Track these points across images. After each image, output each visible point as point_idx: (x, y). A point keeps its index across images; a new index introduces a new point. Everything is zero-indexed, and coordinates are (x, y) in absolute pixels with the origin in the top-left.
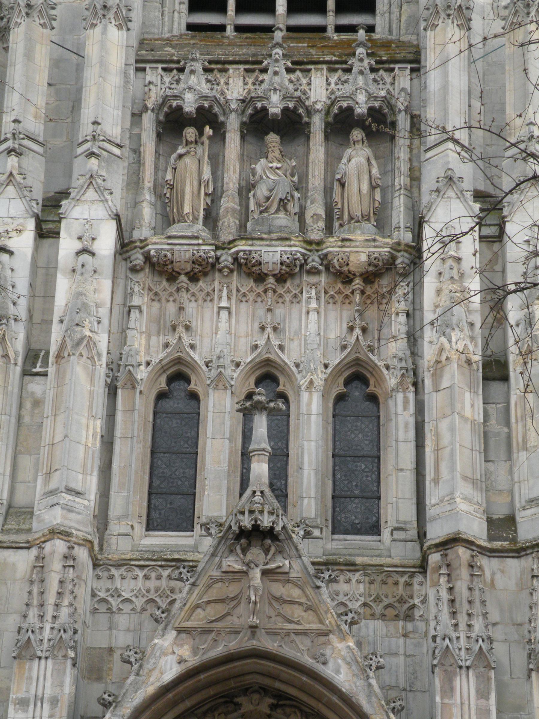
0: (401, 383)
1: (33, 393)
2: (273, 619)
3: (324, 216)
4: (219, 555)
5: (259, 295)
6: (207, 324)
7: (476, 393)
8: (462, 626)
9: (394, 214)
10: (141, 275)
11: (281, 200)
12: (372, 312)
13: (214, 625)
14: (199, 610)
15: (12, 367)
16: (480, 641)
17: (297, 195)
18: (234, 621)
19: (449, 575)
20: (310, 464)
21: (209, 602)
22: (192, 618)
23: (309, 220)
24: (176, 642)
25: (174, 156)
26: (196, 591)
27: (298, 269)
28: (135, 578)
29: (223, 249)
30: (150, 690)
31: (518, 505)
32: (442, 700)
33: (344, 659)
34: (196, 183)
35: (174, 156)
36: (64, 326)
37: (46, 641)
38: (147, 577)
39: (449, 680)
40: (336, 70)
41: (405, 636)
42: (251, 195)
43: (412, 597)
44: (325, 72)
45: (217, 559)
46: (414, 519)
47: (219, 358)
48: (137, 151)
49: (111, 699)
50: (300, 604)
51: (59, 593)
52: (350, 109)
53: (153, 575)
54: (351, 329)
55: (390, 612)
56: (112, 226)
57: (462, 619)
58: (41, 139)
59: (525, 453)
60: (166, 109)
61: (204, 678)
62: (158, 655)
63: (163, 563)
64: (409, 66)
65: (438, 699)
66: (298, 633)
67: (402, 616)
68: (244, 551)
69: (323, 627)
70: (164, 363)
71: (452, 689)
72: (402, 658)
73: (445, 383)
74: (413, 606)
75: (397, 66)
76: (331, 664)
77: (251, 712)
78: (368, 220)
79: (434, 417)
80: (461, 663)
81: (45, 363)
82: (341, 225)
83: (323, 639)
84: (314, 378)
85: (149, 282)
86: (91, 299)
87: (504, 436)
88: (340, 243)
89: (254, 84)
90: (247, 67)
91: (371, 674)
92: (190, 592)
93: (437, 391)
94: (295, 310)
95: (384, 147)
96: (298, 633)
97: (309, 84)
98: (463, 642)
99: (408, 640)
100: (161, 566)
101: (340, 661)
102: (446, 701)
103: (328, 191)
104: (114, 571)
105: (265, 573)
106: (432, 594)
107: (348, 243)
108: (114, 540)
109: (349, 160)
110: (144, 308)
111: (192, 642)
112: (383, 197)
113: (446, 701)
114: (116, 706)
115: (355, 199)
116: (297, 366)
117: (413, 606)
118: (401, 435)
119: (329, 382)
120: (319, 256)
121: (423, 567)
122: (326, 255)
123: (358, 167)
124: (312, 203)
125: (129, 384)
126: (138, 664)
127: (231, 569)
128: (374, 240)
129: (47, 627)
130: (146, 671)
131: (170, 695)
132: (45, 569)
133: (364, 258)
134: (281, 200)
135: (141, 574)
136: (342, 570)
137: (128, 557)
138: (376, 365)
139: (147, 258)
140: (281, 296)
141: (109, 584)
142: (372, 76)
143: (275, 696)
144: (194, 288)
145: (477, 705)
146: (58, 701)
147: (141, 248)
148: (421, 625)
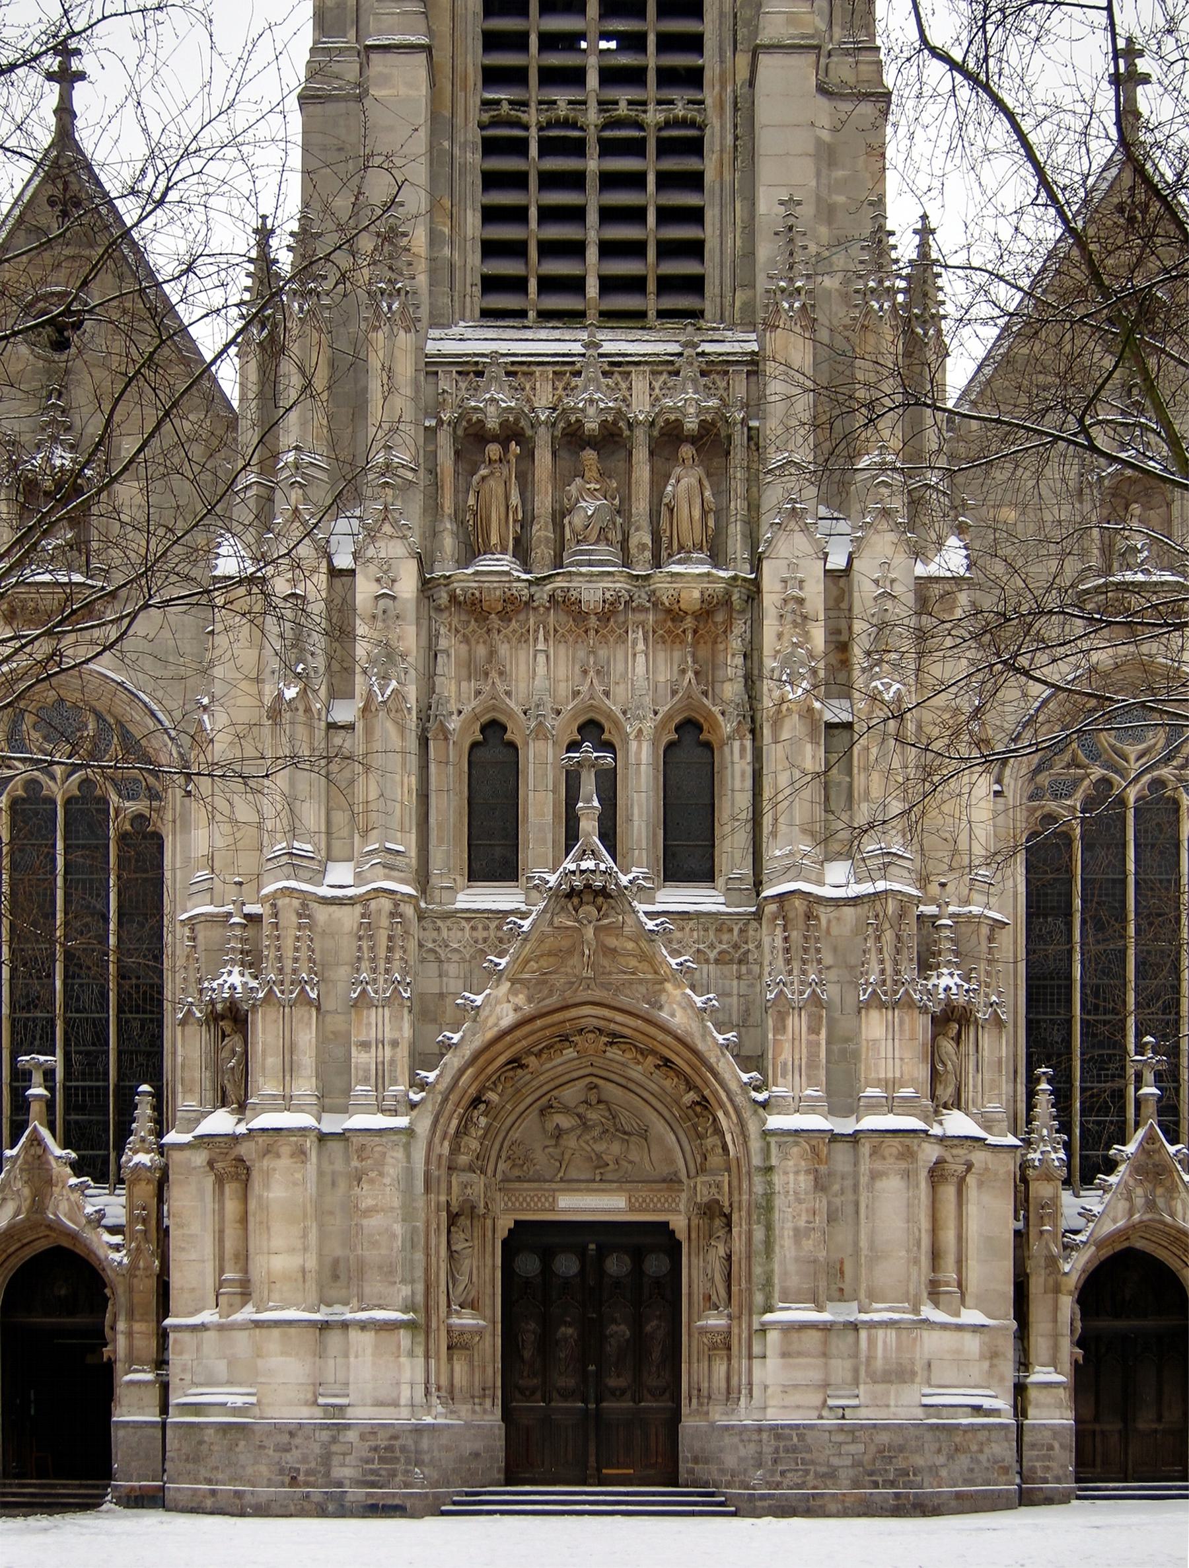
0: (737, 730)
5: (579, 636)
6: (523, 667)
7: (818, 744)
9: (730, 542)
10: (446, 614)
12: (703, 652)
17: (619, 520)
20: (640, 816)
23: (633, 551)
24: (512, 991)
25: (476, 478)
28: (462, 930)
33: (679, 1004)
34: (503, 509)
38: (473, 928)
39: (782, 1017)
40: (661, 373)
41: (739, 978)
42: (566, 521)
47: (538, 706)
48: (432, 471)
52: (678, 424)
53: (480, 926)
54: (683, 672)
56: (412, 565)
57: (796, 965)
65: (770, 1036)
71: (784, 1027)
72: (735, 998)
73: (785, 735)
76: (666, 1008)
78: (701, 549)
82: (670, 556)
83: (658, 987)
87: (845, 785)
89: (565, 389)
92: (522, 946)
93: (776, 742)
95: (717, 462)
97: (630, 389)
103: (654, 516)
104: (439, 923)
106: (766, 940)
109: (678, 481)
112: (717, 521)
115: (685, 525)
118: (738, 786)
119: (659, 729)
121: (758, 916)
122: (654, 592)
123: (689, 489)
124: (637, 530)
133: (696, 594)
139: (453, 597)
140: (604, 636)
142: (704, 380)
143: (608, 1035)
148: (756, 968)
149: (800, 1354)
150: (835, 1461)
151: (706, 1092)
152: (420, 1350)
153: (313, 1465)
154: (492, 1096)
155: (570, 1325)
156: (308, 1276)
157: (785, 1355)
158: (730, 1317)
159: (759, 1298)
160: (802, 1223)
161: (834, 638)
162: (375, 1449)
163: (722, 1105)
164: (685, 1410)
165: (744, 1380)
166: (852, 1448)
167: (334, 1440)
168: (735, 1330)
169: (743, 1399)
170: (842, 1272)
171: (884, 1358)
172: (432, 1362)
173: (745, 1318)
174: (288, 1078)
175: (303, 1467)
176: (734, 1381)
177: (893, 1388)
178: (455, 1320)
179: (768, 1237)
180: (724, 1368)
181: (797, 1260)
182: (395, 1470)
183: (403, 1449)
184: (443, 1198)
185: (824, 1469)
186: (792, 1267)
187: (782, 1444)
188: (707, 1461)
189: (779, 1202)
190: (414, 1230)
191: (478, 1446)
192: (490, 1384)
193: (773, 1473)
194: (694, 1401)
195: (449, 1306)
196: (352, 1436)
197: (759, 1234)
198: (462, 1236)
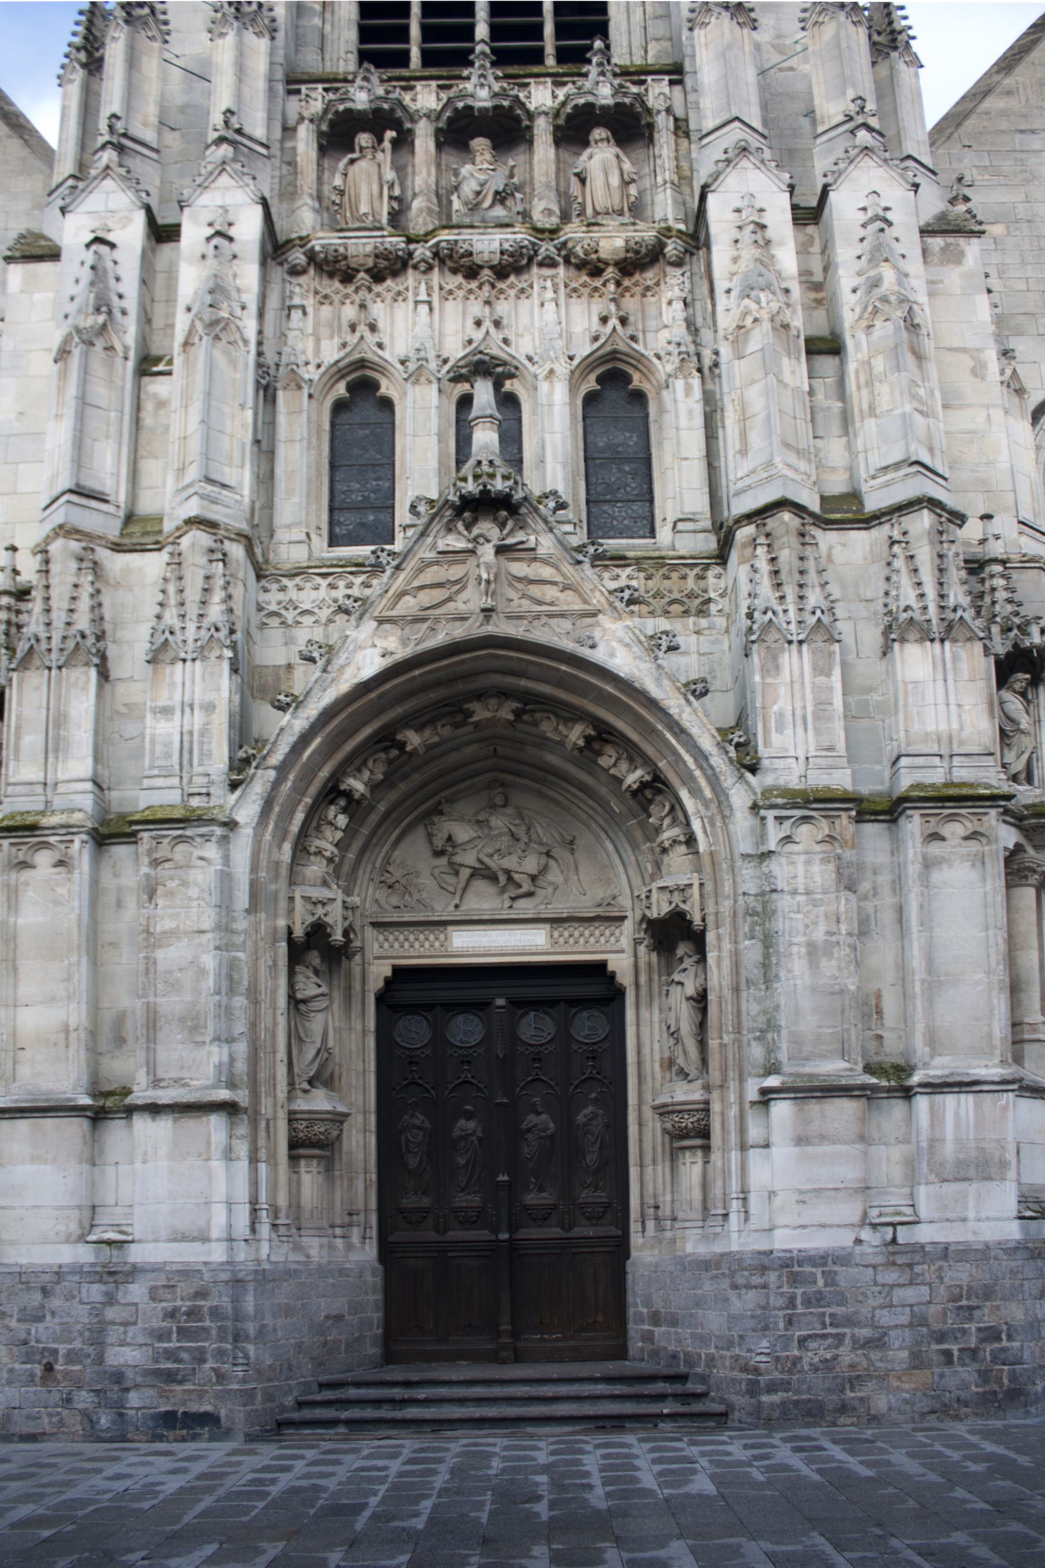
0: (680, 369)
1: (155, 394)
2: (516, 602)
3: (558, 213)
4: (432, 534)
8: (790, 598)
11: (497, 193)
13: (430, 612)
14: (407, 598)
15: (119, 361)
16: (818, 613)
18: (459, 606)
19: (769, 545)
21: (422, 588)
22: (398, 606)
25: (345, 161)
26: (402, 576)
27: (524, 262)
29: (418, 242)
30: (344, 685)
31: (863, 475)
32: (763, 678)
33: (621, 641)
34: (375, 187)
35: (345, 161)
36: (191, 315)
37: (190, 641)
41: (697, 633)
43: (705, 591)
44: (549, 85)
45: (429, 540)
46: (707, 508)
49: (288, 700)
50: (554, 583)
51: (206, 590)
54: (604, 320)
55: (676, 608)
56: (258, 211)
57: (790, 591)
58: (154, 146)
59: (873, 420)
60: (330, 116)
61: (421, 675)
62: (351, 648)
63: (354, 569)
64: (667, 78)
65: (757, 678)
66: (551, 616)
67: (693, 611)
68: (468, 527)
69: (587, 607)
70: (341, 365)
71: (778, 668)
72: (695, 656)
74: (709, 601)
75: (649, 78)
77: (487, 719)
79: (738, 384)
80: (790, 638)
81: (170, 362)
83: (589, 621)
84: (556, 367)
85: (316, 284)
86: (229, 283)
88: (584, 229)
90: (441, 82)
91: (661, 654)
94: (524, 305)
96: (551, 616)
98: (792, 615)
99: (702, 638)
100: (351, 573)
101: (614, 644)
102: (769, 680)
104: (285, 581)
105: (500, 550)
107: (596, 228)
108: (283, 549)
110: (310, 310)
111: (399, 632)
113: (769, 680)
114: (297, 708)
116: (530, 359)
117: (709, 601)
118: (683, 422)
120: (555, 247)
122: (564, 244)
125: (293, 384)
126: (324, 659)
127: (450, 549)
128: (634, 224)
129: (191, 627)
130: (336, 667)
131: (373, 695)
132: (184, 565)
133: (620, 243)
134: (497, 193)
135: (324, 583)
136: (606, 566)
137: (305, 565)
138: (642, 355)
139: (311, 256)
141: (281, 596)
143: (518, 700)
144: (378, 288)
145: (813, 683)
146: (214, 707)
147: (302, 247)
149: (823, 1138)
150: (885, 1318)
151: (662, 764)
152: (242, 1149)
153: (77, 1344)
154: (357, 785)
155: (469, 1116)
156: (73, 1035)
157: (800, 1141)
158: (707, 1088)
159: (756, 1052)
160: (819, 934)
161: (804, 279)
162: (172, 1314)
163: (688, 780)
164: (636, 1239)
165: (734, 1185)
166: (910, 1294)
167: (111, 1300)
168: (716, 1107)
169: (733, 1217)
170: (879, 1012)
171: (957, 1140)
172: (263, 1167)
173: (733, 1085)
174: (51, 760)
175: (63, 1348)
176: (717, 1191)
177: (972, 1188)
178: (302, 1104)
179: (766, 956)
180: (697, 1169)
181: (814, 989)
182: (202, 1351)
183: (215, 1313)
184: (282, 923)
185: (865, 1333)
186: (806, 1003)
187: (799, 1292)
188: (673, 1322)
189: (784, 903)
190: (233, 965)
191: (340, 1304)
192: (361, 1206)
193: (787, 1340)
194: (650, 1224)
195: (291, 1084)
196: (137, 1291)
197: (752, 952)
198: (314, 979)
